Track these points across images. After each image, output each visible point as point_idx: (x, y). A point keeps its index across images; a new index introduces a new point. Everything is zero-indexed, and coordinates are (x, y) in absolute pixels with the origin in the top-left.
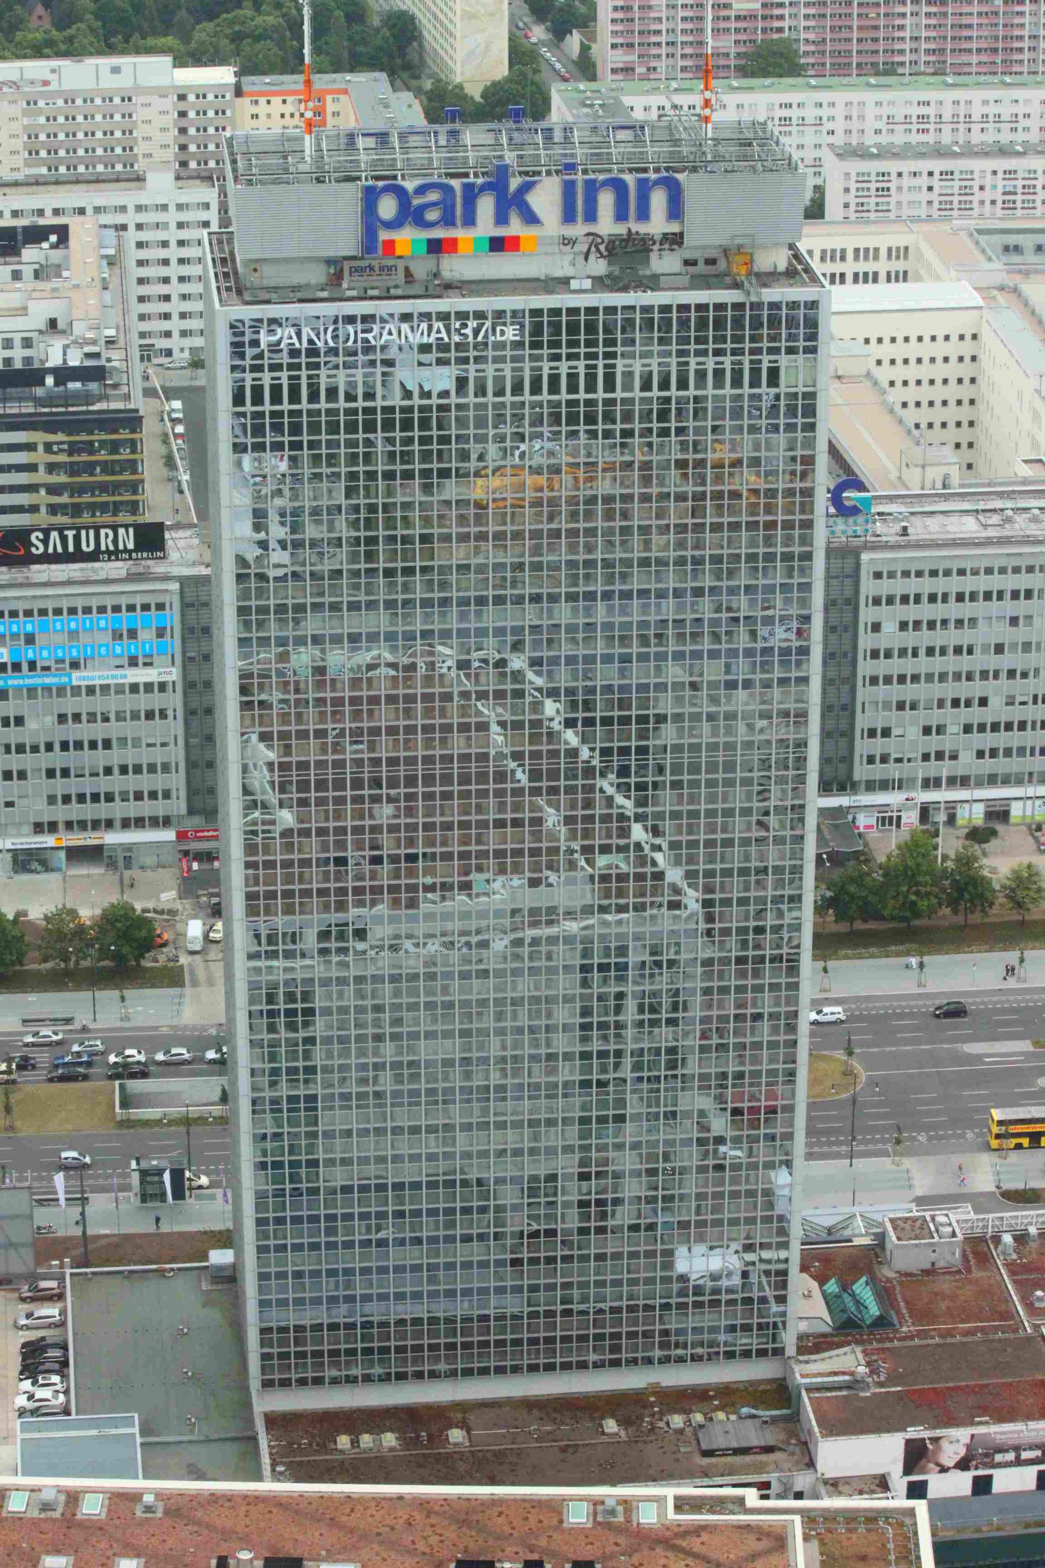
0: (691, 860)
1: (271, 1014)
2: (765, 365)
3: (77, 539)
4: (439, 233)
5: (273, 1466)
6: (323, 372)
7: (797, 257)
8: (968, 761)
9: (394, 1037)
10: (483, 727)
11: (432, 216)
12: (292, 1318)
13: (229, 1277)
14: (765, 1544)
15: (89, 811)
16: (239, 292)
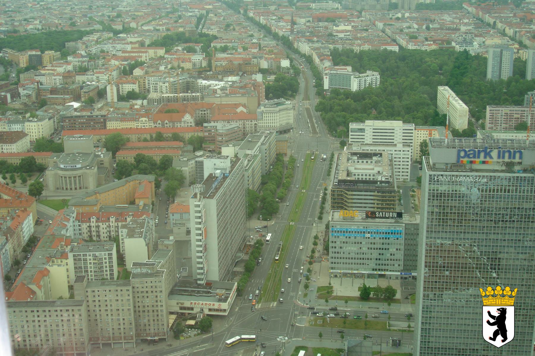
4: (472, 159)
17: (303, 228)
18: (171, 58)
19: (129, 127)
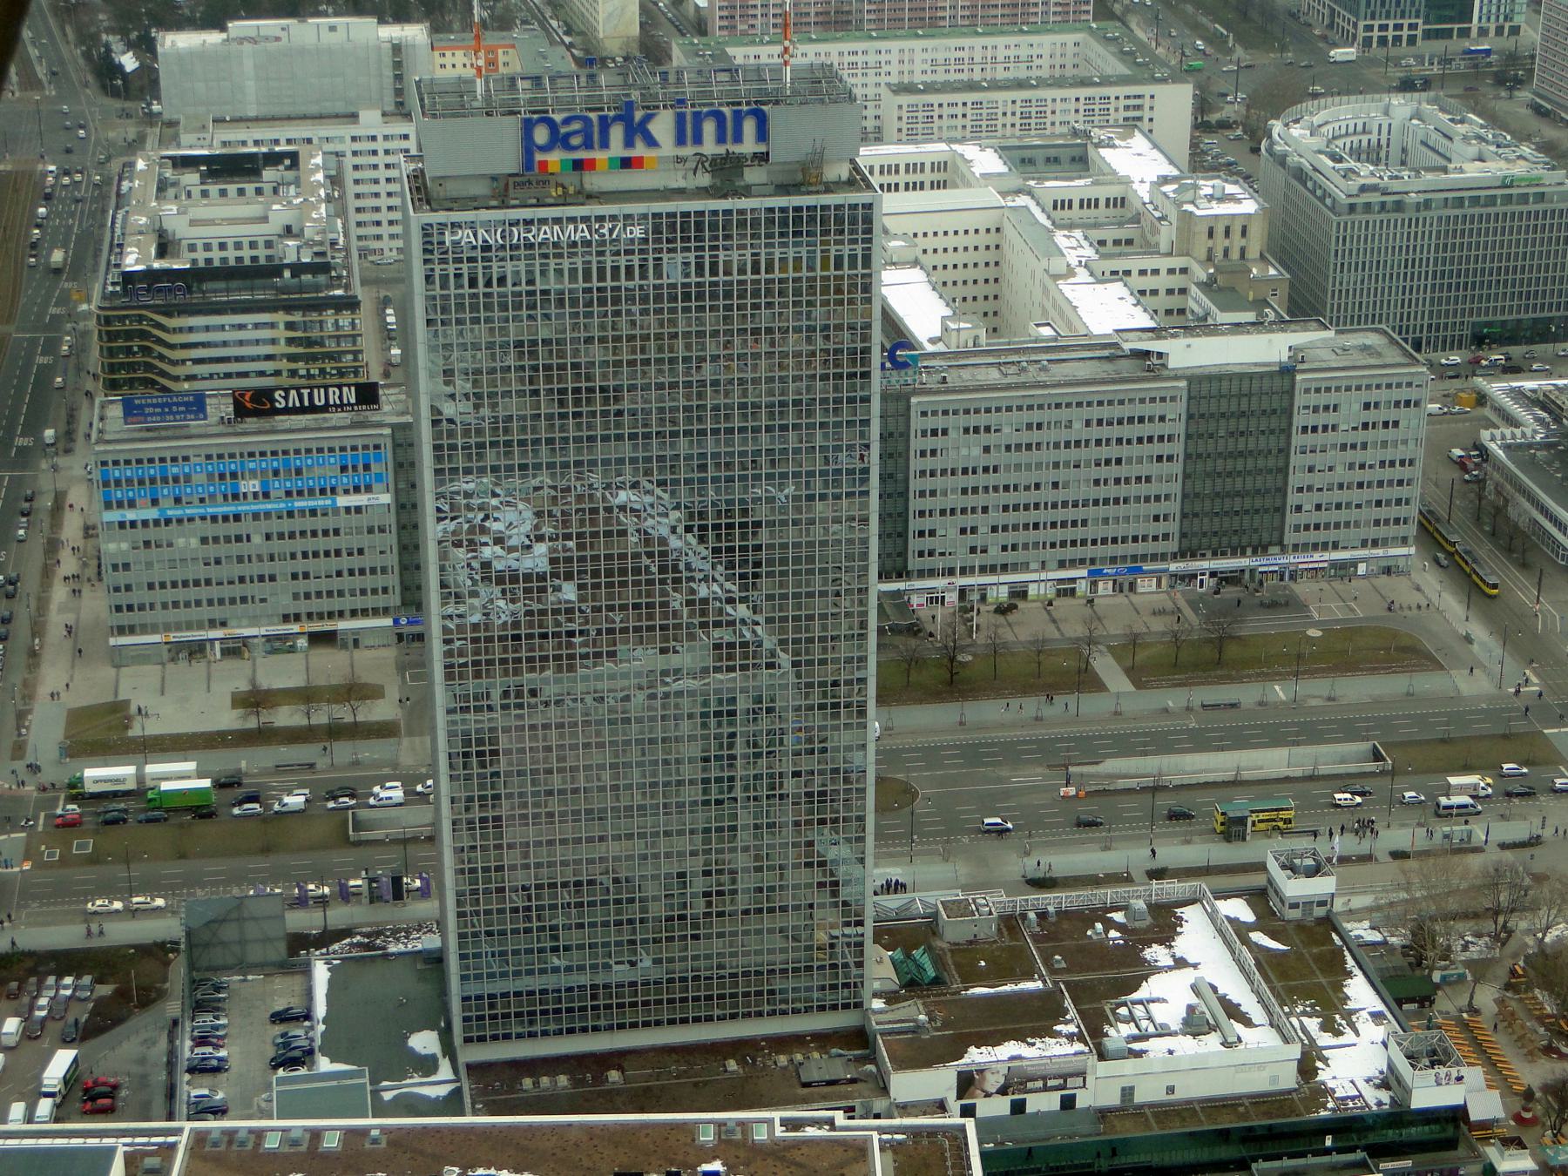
0: (783, 630)
1: (466, 755)
2: (833, 253)
3: (311, 396)
5: (473, 1104)
6: (495, 265)
7: (856, 169)
8: (995, 555)
9: (560, 770)
10: (623, 533)
12: (487, 988)
13: (435, 960)
14: (850, 1154)
15: (325, 605)
16: (428, 202)
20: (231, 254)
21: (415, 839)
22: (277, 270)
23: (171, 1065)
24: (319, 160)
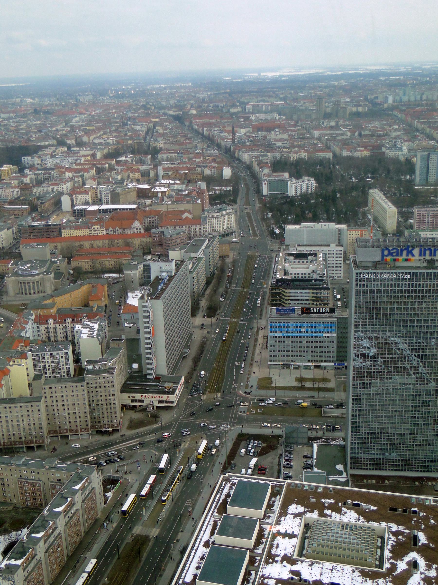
11: (394, 254)
12: (357, 456)
13: (344, 448)
15: (318, 359)
17: (245, 324)
18: (121, 169)
19: (79, 234)
20: (300, 276)
21: (338, 417)
22: (311, 280)
23: (279, 464)
24: (321, 255)
